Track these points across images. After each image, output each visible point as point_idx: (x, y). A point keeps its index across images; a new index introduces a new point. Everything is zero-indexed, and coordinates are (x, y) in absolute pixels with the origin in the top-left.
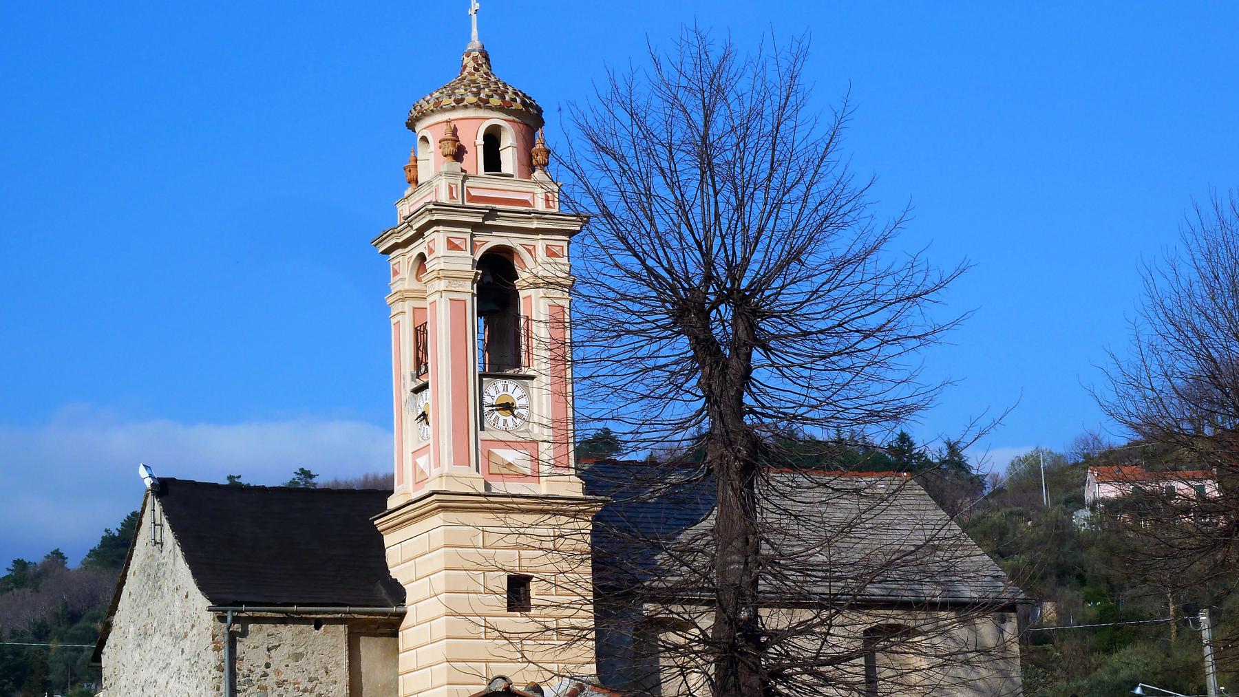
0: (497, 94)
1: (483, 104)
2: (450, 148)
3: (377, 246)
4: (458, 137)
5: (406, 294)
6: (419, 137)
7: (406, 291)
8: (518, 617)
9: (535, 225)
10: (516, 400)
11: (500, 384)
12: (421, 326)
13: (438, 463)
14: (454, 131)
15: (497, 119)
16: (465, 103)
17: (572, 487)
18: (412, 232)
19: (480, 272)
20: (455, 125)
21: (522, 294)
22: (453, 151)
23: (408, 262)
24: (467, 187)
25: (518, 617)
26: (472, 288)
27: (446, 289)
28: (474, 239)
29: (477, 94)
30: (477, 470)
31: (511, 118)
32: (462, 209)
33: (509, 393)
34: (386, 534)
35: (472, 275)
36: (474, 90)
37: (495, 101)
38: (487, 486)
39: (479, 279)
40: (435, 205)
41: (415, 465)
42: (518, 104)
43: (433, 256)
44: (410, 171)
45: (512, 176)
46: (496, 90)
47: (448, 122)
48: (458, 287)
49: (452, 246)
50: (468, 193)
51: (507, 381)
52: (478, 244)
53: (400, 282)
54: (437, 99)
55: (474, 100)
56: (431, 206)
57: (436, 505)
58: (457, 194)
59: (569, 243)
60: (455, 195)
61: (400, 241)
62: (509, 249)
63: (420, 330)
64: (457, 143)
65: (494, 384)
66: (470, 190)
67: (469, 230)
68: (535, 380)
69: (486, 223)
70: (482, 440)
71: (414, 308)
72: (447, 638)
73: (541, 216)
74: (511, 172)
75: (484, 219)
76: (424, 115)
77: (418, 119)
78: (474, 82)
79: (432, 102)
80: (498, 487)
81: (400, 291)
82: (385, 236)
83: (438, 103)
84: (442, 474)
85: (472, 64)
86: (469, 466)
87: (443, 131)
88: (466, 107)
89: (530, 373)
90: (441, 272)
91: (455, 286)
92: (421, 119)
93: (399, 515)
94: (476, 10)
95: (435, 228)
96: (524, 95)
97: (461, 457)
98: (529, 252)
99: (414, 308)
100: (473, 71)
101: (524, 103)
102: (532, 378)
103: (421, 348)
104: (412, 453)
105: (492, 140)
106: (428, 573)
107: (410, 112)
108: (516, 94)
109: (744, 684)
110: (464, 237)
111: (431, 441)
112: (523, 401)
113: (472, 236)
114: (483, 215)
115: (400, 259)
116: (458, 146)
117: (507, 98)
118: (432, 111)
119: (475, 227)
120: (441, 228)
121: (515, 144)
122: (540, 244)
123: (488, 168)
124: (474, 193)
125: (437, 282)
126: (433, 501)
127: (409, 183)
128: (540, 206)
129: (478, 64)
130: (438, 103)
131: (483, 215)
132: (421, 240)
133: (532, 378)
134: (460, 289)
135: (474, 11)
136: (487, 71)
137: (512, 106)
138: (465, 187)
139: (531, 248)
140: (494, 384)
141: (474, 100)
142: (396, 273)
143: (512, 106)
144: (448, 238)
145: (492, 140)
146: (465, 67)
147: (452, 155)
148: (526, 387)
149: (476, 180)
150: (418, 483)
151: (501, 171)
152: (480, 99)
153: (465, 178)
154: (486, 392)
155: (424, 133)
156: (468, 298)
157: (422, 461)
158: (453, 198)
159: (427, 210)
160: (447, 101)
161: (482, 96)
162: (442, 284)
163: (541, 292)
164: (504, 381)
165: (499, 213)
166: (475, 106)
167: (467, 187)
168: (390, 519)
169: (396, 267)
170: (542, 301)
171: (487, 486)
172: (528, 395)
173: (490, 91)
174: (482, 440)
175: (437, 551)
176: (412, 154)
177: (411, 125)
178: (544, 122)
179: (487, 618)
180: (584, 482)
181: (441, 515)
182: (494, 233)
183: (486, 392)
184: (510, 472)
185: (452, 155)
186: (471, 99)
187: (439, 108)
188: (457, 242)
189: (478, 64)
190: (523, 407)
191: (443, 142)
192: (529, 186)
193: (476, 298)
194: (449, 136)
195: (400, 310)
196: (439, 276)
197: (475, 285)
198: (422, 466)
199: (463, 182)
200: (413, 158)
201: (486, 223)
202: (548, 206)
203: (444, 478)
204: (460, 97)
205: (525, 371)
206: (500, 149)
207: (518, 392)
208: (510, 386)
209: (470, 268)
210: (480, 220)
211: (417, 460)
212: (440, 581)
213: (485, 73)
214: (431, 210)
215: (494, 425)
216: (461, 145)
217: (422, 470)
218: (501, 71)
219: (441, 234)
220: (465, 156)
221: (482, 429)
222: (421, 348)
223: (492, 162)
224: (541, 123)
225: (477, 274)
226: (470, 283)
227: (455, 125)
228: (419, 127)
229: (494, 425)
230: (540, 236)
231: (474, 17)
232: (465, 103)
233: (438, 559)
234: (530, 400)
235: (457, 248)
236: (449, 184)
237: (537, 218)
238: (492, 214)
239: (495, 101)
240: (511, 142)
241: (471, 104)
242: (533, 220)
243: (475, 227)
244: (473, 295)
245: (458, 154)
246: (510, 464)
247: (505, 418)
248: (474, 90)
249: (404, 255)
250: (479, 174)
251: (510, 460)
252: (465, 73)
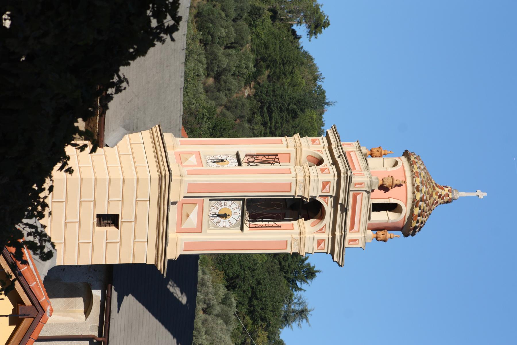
0: (422, 212)
1: (415, 203)
2: (387, 183)
3: (331, 129)
4: (395, 187)
5: (299, 149)
6: (398, 160)
7: (301, 149)
8: (93, 220)
9: (338, 234)
10: (228, 220)
11: (239, 210)
12: (278, 159)
13: (190, 173)
14: (400, 185)
15: (406, 211)
16: (416, 192)
17: (173, 254)
18: (336, 156)
19: (308, 201)
20: (403, 185)
21: (295, 223)
22: (385, 185)
23: (319, 151)
24: (362, 193)
25: (93, 220)
26: (298, 196)
27: (298, 181)
28: (329, 197)
29: (422, 200)
30: (184, 197)
31: (406, 220)
32: (348, 190)
33: (233, 216)
34: (150, 132)
35: (306, 196)
36: (425, 198)
37: (417, 211)
38: (174, 203)
39: (304, 200)
40: (350, 176)
41: (191, 154)
42: (414, 224)
43: (319, 171)
44: (378, 151)
45: (369, 219)
46: (424, 211)
47: (405, 182)
48: (299, 188)
49: (325, 184)
50: (359, 194)
51: (240, 215)
52: (326, 199)
53: (307, 144)
54: (420, 174)
55: (418, 198)
56: (349, 174)
57: (163, 175)
58: (358, 187)
59: (327, 253)
60: (357, 186)
61: (333, 146)
62: (323, 217)
63: (276, 158)
64: (390, 188)
65: (238, 207)
66: (361, 195)
67: (334, 195)
68: (241, 231)
69: (339, 205)
70: (203, 200)
71: (290, 154)
72: (81, 179)
73: (343, 238)
74: (371, 219)
75: (341, 204)
76: (411, 165)
77: (409, 160)
78: (431, 196)
79: (418, 170)
80: (174, 210)
81: (301, 145)
82: (337, 136)
83: (418, 175)
84: (183, 176)
85: (443, 193)
86: (188, 193)
87: (399, 179)
88: (414, 193)
89: (245, 227)
90: (308, 178)
91: (300, 186)
92: (409, 162)
93: (160, 145)
94: (479, 196)
95: (336, 174)
96: (421, 227)
97: (192, 187)
98: (321, 229)
99: (290, 154)
100: (439, 194)
101: (416, 228)
102: (242, 229)
103: (264, 159)
104: (199, 152)
105: (393, 207)
106: (123, 165)
107: (415, 154)
108: (422, 223)
109: (216, 8)
110: (330, 192)
111: (205, 168)
112: (227, 224)
113: (331, 196)
114: (343, 204)
115: (322, 145)
116: (389, 188)
117: (419, 218)
118: (412, 171)
119: (336, 199)
120: (336, 178)
121: (390, 222)
122: (326, 236)
123: (374, 205)
124: (359, 197)
125: (303, 175)
126: (166, 173)
127: (371, 150)
128: (350, 236)
129: (443, 197)
130: (418, 175)
131: (343, 204)
132: (331, 162)
133: (242, 229)
134: (298, 189)
135: (478, 195)
136: (439, 202)
137: (413, 221)
138: (362, 192)
139: (323, 230)
140: (238, 207)
141: (418, 198)
142: (313, 141)
143: (413, 221)
144: (330, 182)
145: (393, 207)
146: (442, 189)
147: (383, 184)
148: (235, 226)
149: (367, 198)
150: (179, 156)
151: (372, 211)
152: (418, 202)
153: (368, 192)
154: (233, 202)
155: (400, 164)
156: (292, 193)
157: (193, 160)
158: (356, 185)
159: (347, 171)
160: (418, 181)
161: (420, 203)
162: (301, 178)
163: (297, 236)
164: (240, 213)
165: (345, 213)
166: (414, 199)
167: (362, 193)
168: (158, 138)
169: (317, 141)
170: (290, 236)
171: (174, 203)
172: (232, 227)
173: (424, 208)
174: (203, 200)
175: (135, 173)
176: (389, 152)
177: (406, 154)
178: (407, 237)
179: (93, 202)
180: (176, 259)
181: (158, 177)
182: (332, 209)
183: (233, 202)
184: (183, 216)
185: (383, 184)
186: (419, 196)
187: (414, 175)
188: (327, 187)
189: (443, 197)
190: (224, 223)
191: (391, 179)
192: (363, 230)
193: (292, 197)
194: (395, 182)
195: (289, 145)
196: (306, 176)
197: (300, 197)
198: (189, 159)
199: (366, 191)
200: (386, 152)
201: (339, 205)
202: (350, 241)
203: (180, 178)
204: (420, 189)
205: (247, 224)
206: (388, 211)
207: (233, 221)
208: (238, 216)
209: (311, 194)
210: (340, 202)
211: (194, 156)
212: (116, 174)
213: (437, 202)
214: (347, 173)
215: (213, 207)
216: (389, 190)
217: (188, 159)
218: (439, 211)
219: (332, 178)
220: (382, 191)
221: (210, 200)
222: (264, 159)
223: (377, 207)
224: (406, 235)
225: (307, 199)
226: (301, 194)
227: (403, 185)
228: (404, 159)
229: (213, 207)
230: (331, 236)
231: (474, 194)
232: (416, 192)
233: (130, 174)
234: (229, 228)
235: (324, 187)
236: (364, 183)
237: (341, 236)
238: (344, 210)
239: (417, 211)
240: (391, 219)
241: (415, 197)
242: (340, 233)
243: (336, 199)
244: (294, 196)
245: (383, 188)
246: (188, 216)
247: (219, 209)
248: (425, 198)
249: (324, 148)
250: (370, 200)
251: (191, 216)
252: (437, 189)
